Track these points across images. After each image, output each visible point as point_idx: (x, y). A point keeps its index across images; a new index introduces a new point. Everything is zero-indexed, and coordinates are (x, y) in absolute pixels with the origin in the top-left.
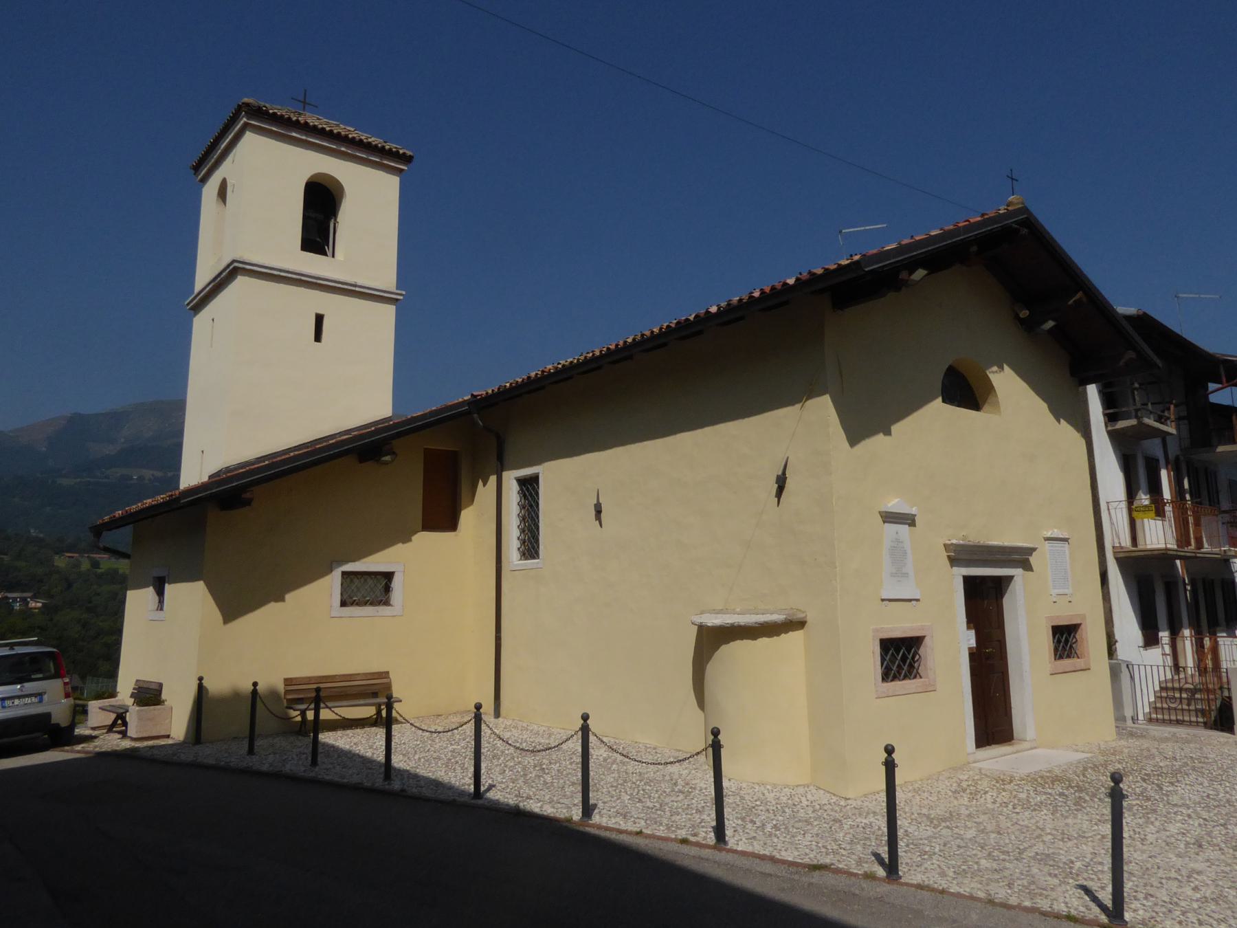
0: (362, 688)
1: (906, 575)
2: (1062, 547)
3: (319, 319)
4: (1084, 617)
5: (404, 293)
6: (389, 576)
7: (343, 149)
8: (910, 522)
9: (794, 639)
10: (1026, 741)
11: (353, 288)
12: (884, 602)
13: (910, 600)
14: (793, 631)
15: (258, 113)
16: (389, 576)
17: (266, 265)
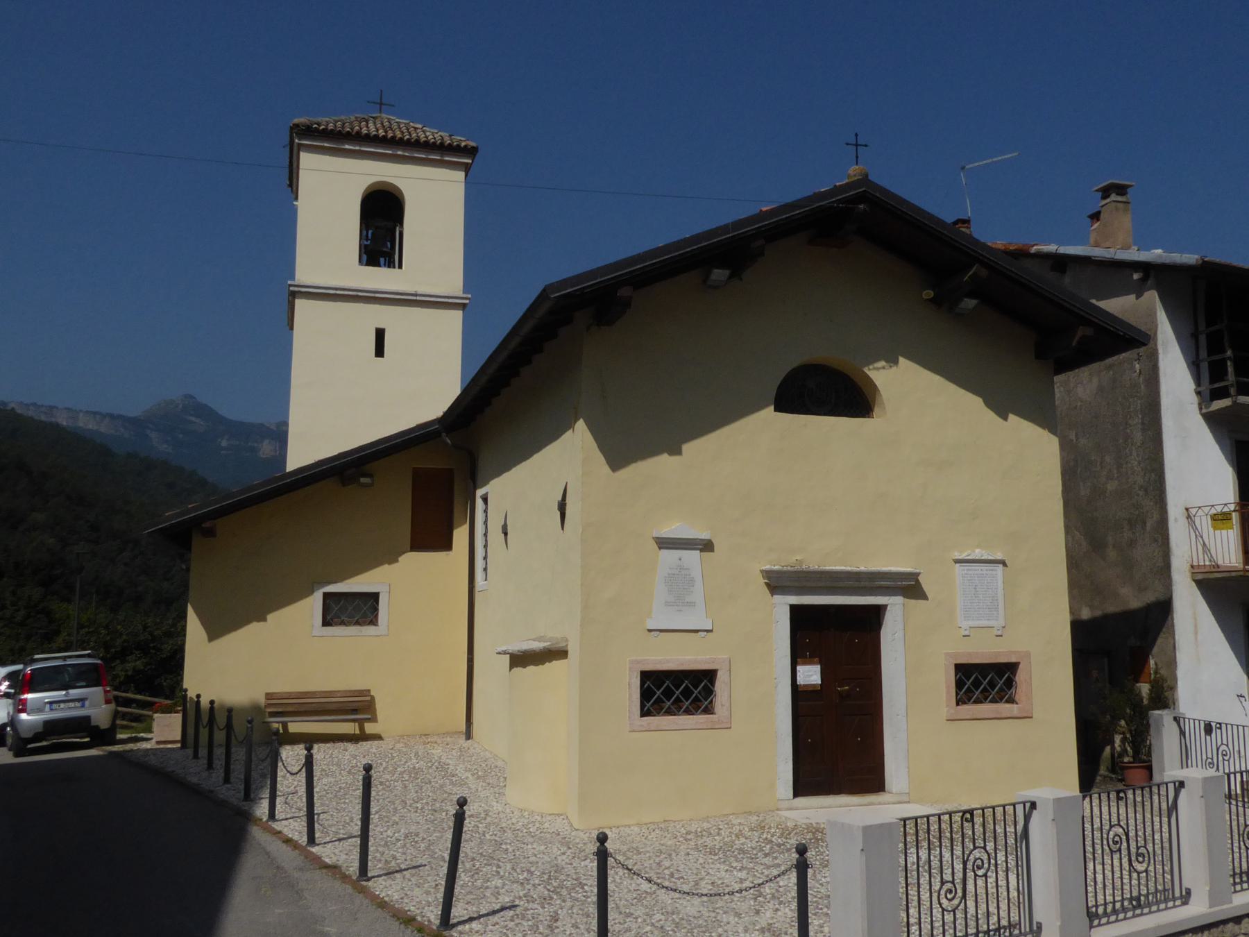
0: (360, 704)
1: (693, 604)
2: (992, 570)
3: (380, 334)
4: (1028, 655)
5: (470, 296)
6: (375, 597)
7: (399, 153)
8: (701, 547)
9: (556, 665)
10: (892, 793)
11: (415, 298)
12: (653, 633)
13: (697, 631)
14: (556, 660)
15: (308, 131)
16: (375, 597)
17: (321, 285)
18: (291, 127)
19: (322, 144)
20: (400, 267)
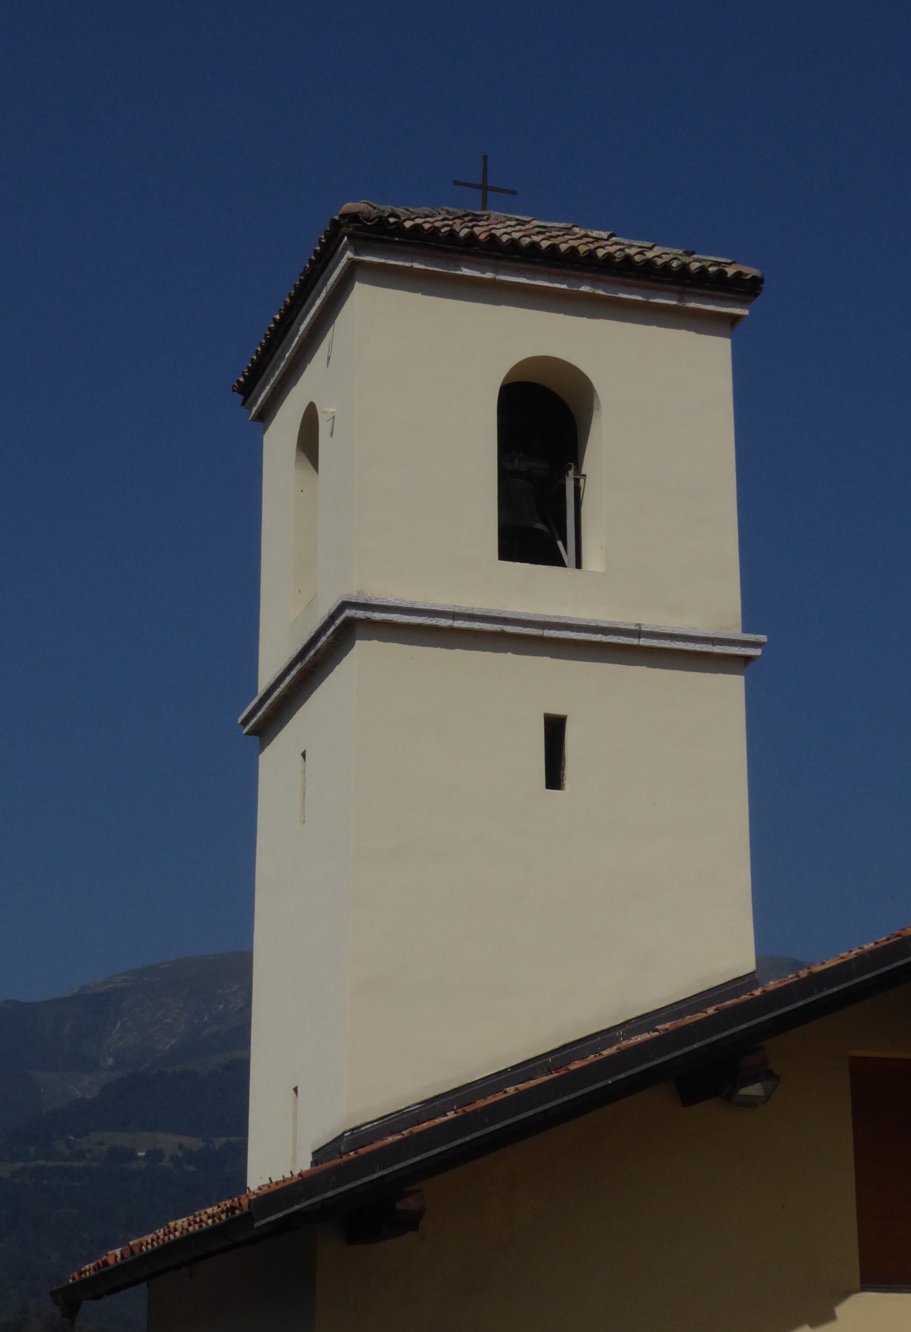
5: (763, 638)
7: (585, 289)
11: (635, 641)
18: (334, 221)
19: (408, 264)
20: (579, 565)
